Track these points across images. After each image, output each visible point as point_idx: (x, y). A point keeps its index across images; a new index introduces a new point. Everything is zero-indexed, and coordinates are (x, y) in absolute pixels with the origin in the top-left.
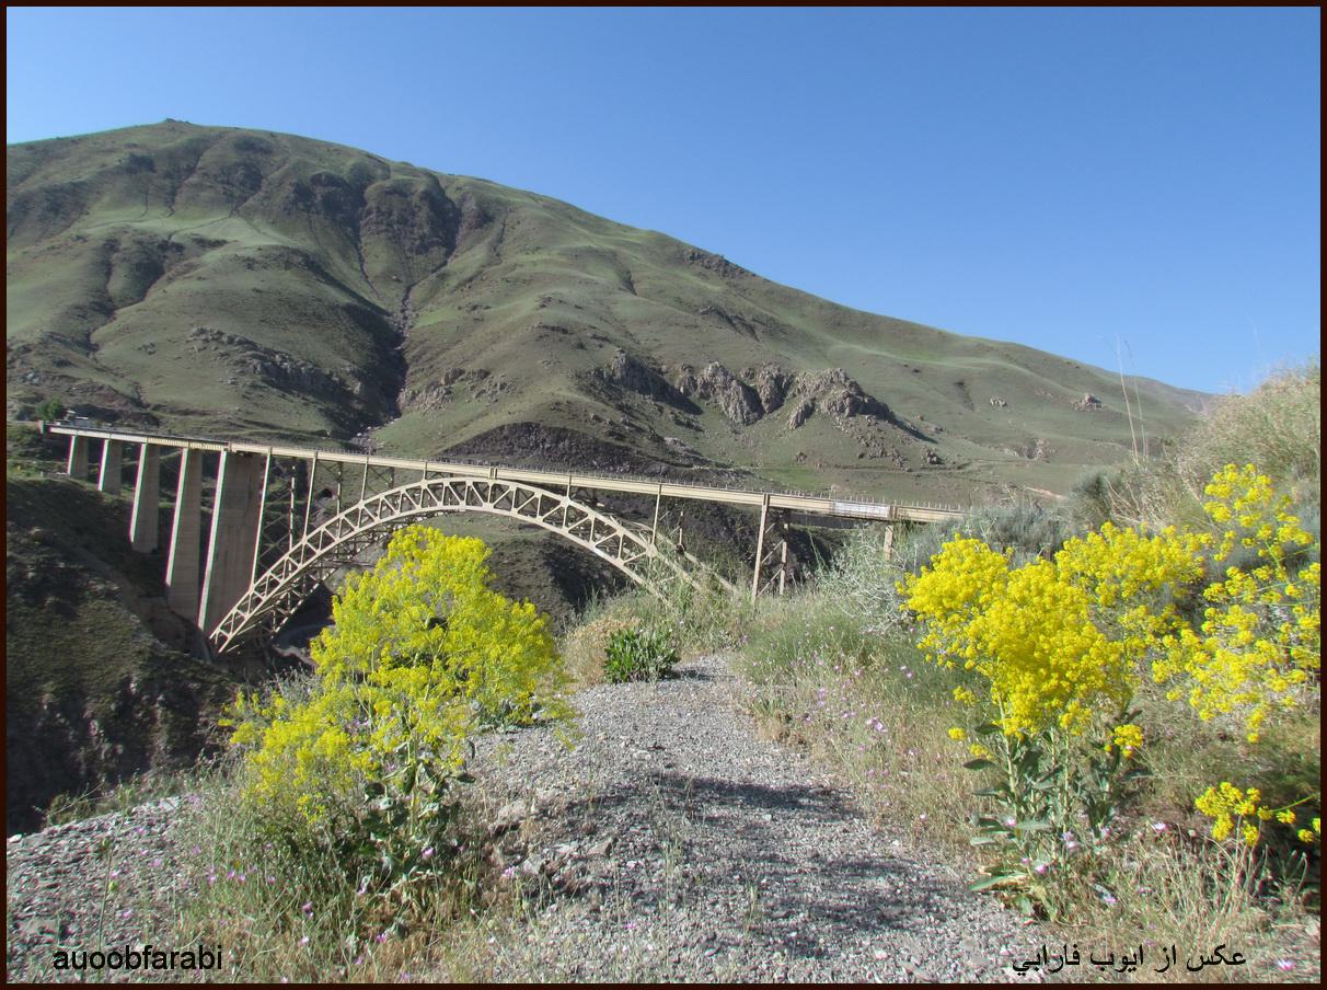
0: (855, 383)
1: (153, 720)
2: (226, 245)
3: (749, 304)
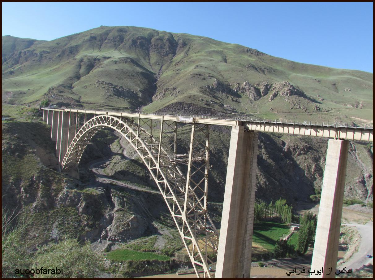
0: (292, 85)
2: (111, 58)
3: (264, 63)
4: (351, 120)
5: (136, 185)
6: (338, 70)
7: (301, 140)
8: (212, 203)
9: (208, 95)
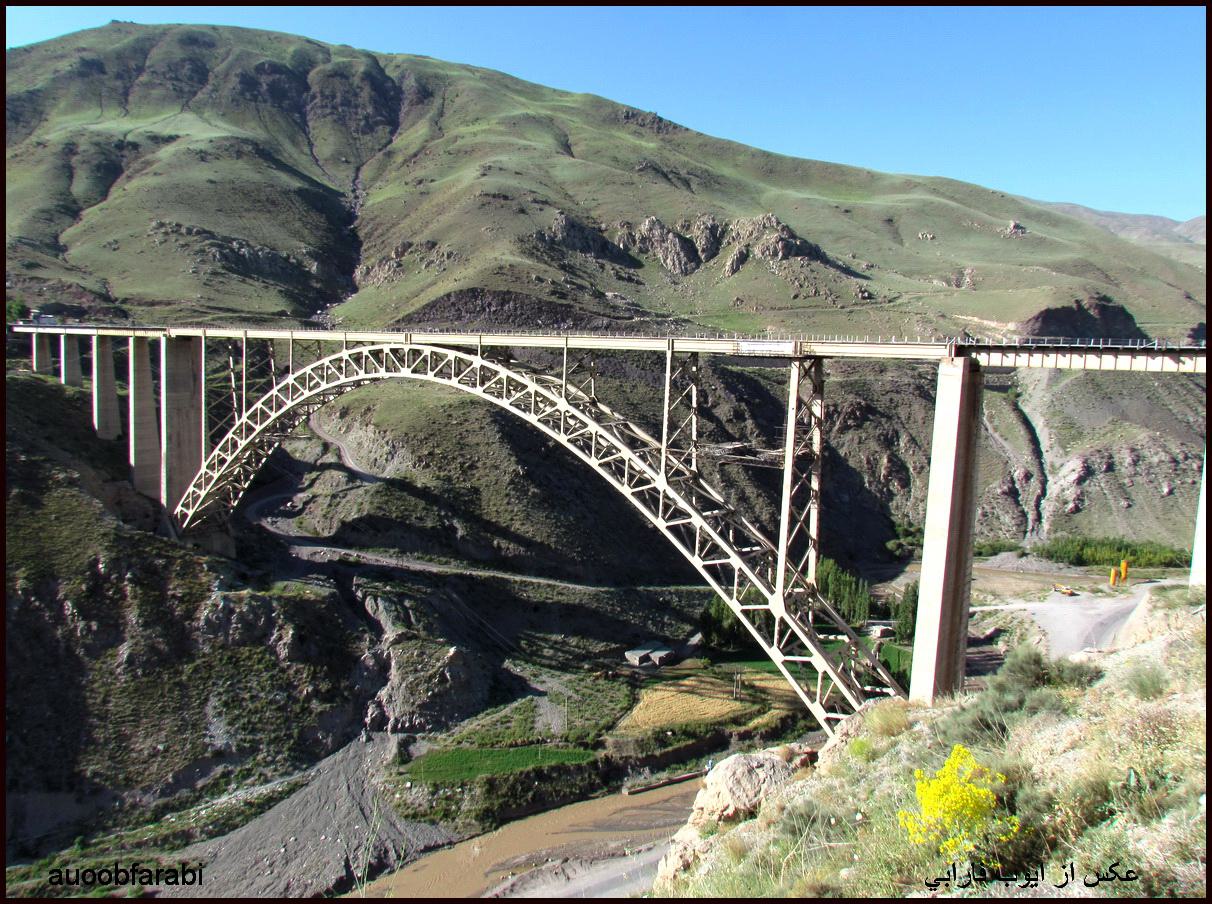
1: (124, 597)
2: (179, 141)
4: (956, 324)
5: (418, 558)
6: (891, 177)
7: (843, 387)
8: (651, 588)
9: (546, 263)
